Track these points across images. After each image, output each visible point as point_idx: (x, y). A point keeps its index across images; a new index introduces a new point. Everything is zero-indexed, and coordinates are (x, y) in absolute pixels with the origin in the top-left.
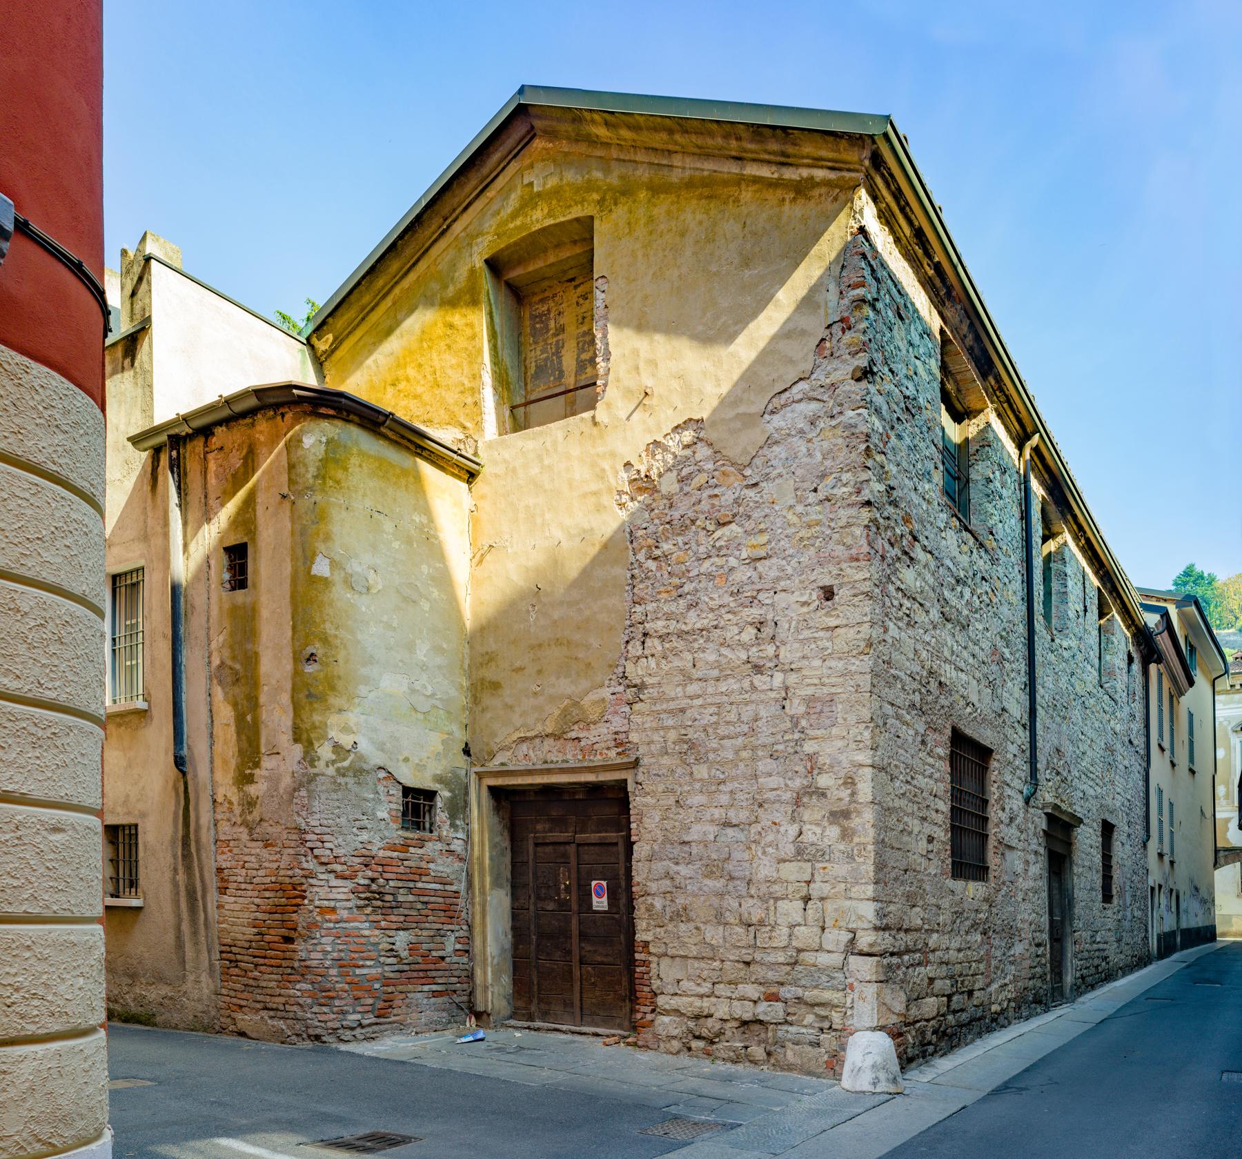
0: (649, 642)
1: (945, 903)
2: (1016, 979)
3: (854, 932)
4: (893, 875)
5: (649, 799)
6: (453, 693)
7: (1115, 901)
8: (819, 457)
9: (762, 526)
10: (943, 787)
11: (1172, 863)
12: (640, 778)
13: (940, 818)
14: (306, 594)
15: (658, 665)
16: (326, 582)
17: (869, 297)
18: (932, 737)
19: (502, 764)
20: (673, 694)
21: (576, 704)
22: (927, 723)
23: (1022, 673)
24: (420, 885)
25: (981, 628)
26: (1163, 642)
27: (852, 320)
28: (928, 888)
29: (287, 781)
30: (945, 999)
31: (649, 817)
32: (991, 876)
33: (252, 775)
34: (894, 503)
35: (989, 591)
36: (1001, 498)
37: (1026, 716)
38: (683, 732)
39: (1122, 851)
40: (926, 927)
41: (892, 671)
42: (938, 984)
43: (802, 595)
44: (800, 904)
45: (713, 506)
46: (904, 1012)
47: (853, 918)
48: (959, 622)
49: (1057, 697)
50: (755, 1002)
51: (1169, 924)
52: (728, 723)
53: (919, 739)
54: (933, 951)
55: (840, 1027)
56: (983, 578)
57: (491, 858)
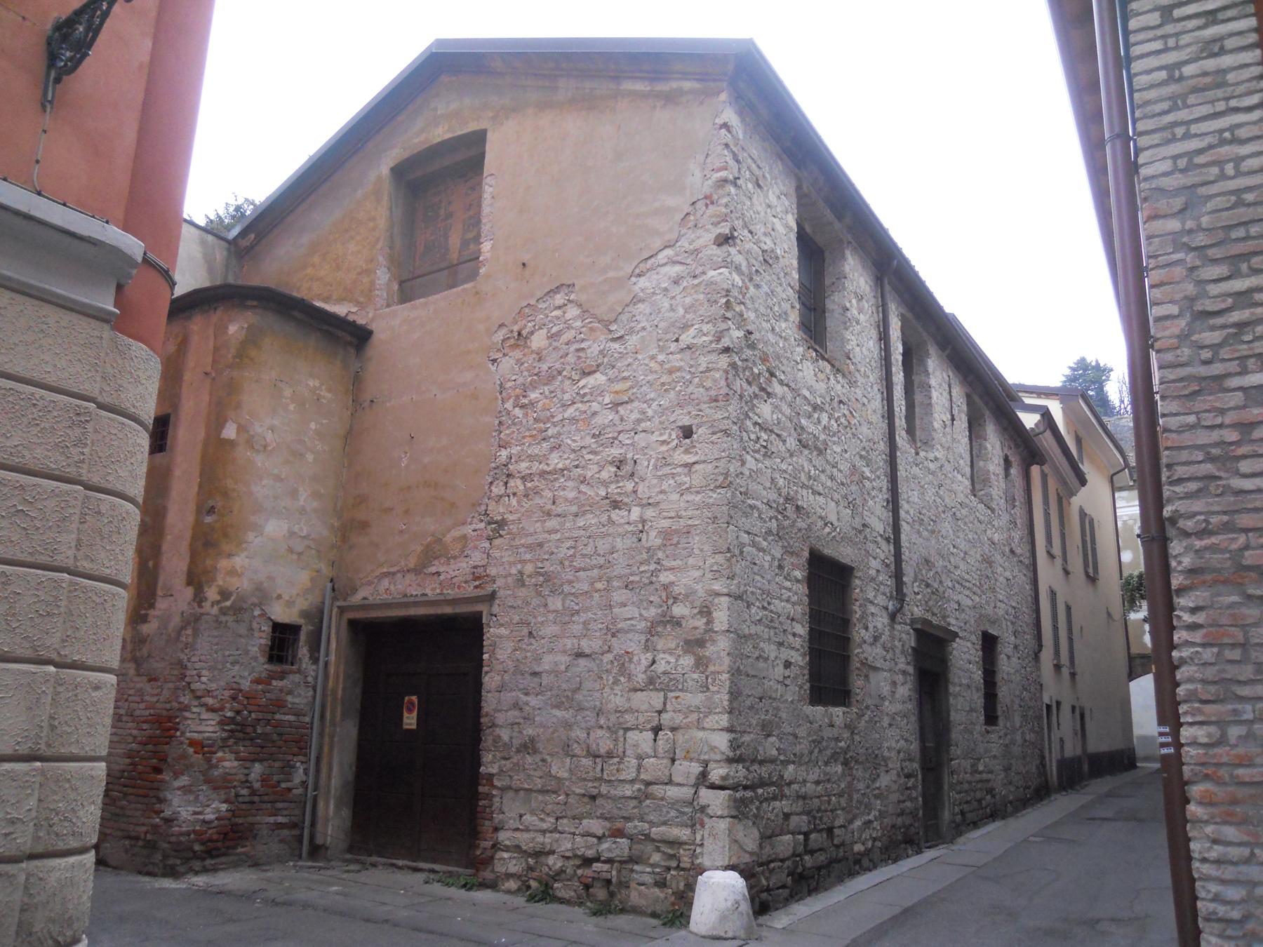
0: (512, 483)
1: (802, 732)
2: (882, 815)
3: (706, 764)
4: (748, 703)
5: (503, 631)
6: (325, 533)
7: (1001, 721)
8: (681, 311)
9: (625, 374)
10: (800, 610)
11: (1073, 675)
12: (495, 609)
13: (797, 642)
14: (216, 455)
15: (518, 502)
16: (232, 443)
17: (731, 177)
18: (789, 560)
19: (365, 598)
20: (532, 530)
21: (439, 541)
22: (783, 547)
23: (884, 490)
24: (277, 716)
25: (839, 450)
26: (1047, 441)
27: (715, 197)
28: (784, 715)
29: (176, 621)
30: (801, 837)
31: (501, 645)
32: (853, 700)
33: (146, 615)
34: (752, 346)
35: (847, 412)
36: (858, 323)
37: (890, 530)
38: (540, 565)
39: (1008, 665)
40: (782, 758)
41: (749, 501)
42: (794, 820)
43: (661, 435)
44: (650, 735)
45: (579, 358)
46: (756, 850)
47: (706, 749)
48: (816, 448)
49: (924, 511)
50: (599, 838)
51: (1072, 749)
52: (584, 556)
53: (776, 563)
54: (789, 784)
55: (688, 866)
56: (841, 402)
57: (344, 690)
